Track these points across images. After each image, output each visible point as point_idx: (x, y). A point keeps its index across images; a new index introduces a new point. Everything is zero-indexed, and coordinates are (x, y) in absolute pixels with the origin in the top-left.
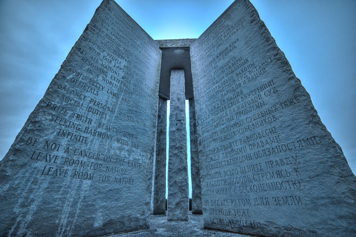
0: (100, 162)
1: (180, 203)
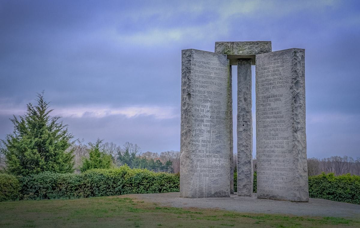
0: (210, 169)
1: (246, 186)
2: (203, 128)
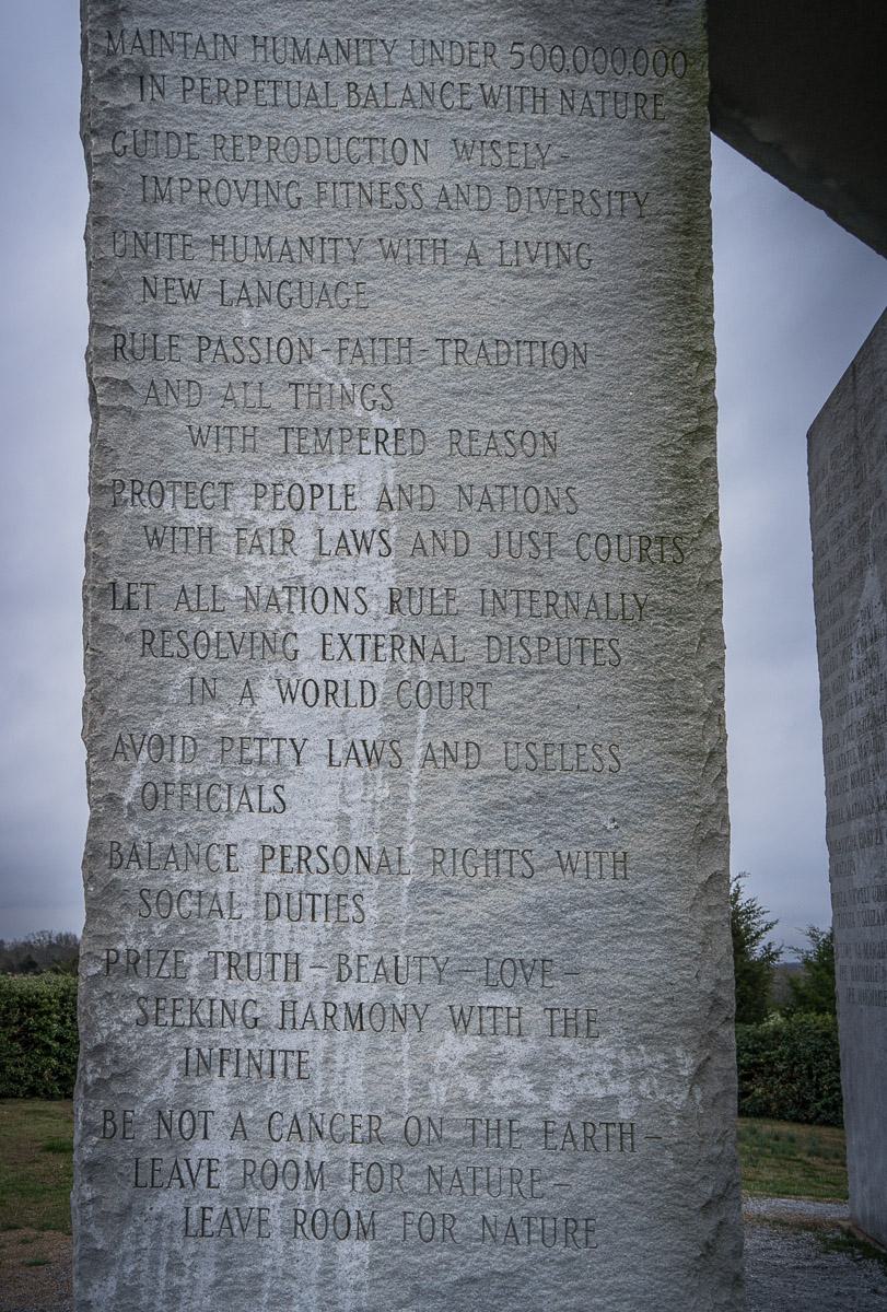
2: (274, 714)
